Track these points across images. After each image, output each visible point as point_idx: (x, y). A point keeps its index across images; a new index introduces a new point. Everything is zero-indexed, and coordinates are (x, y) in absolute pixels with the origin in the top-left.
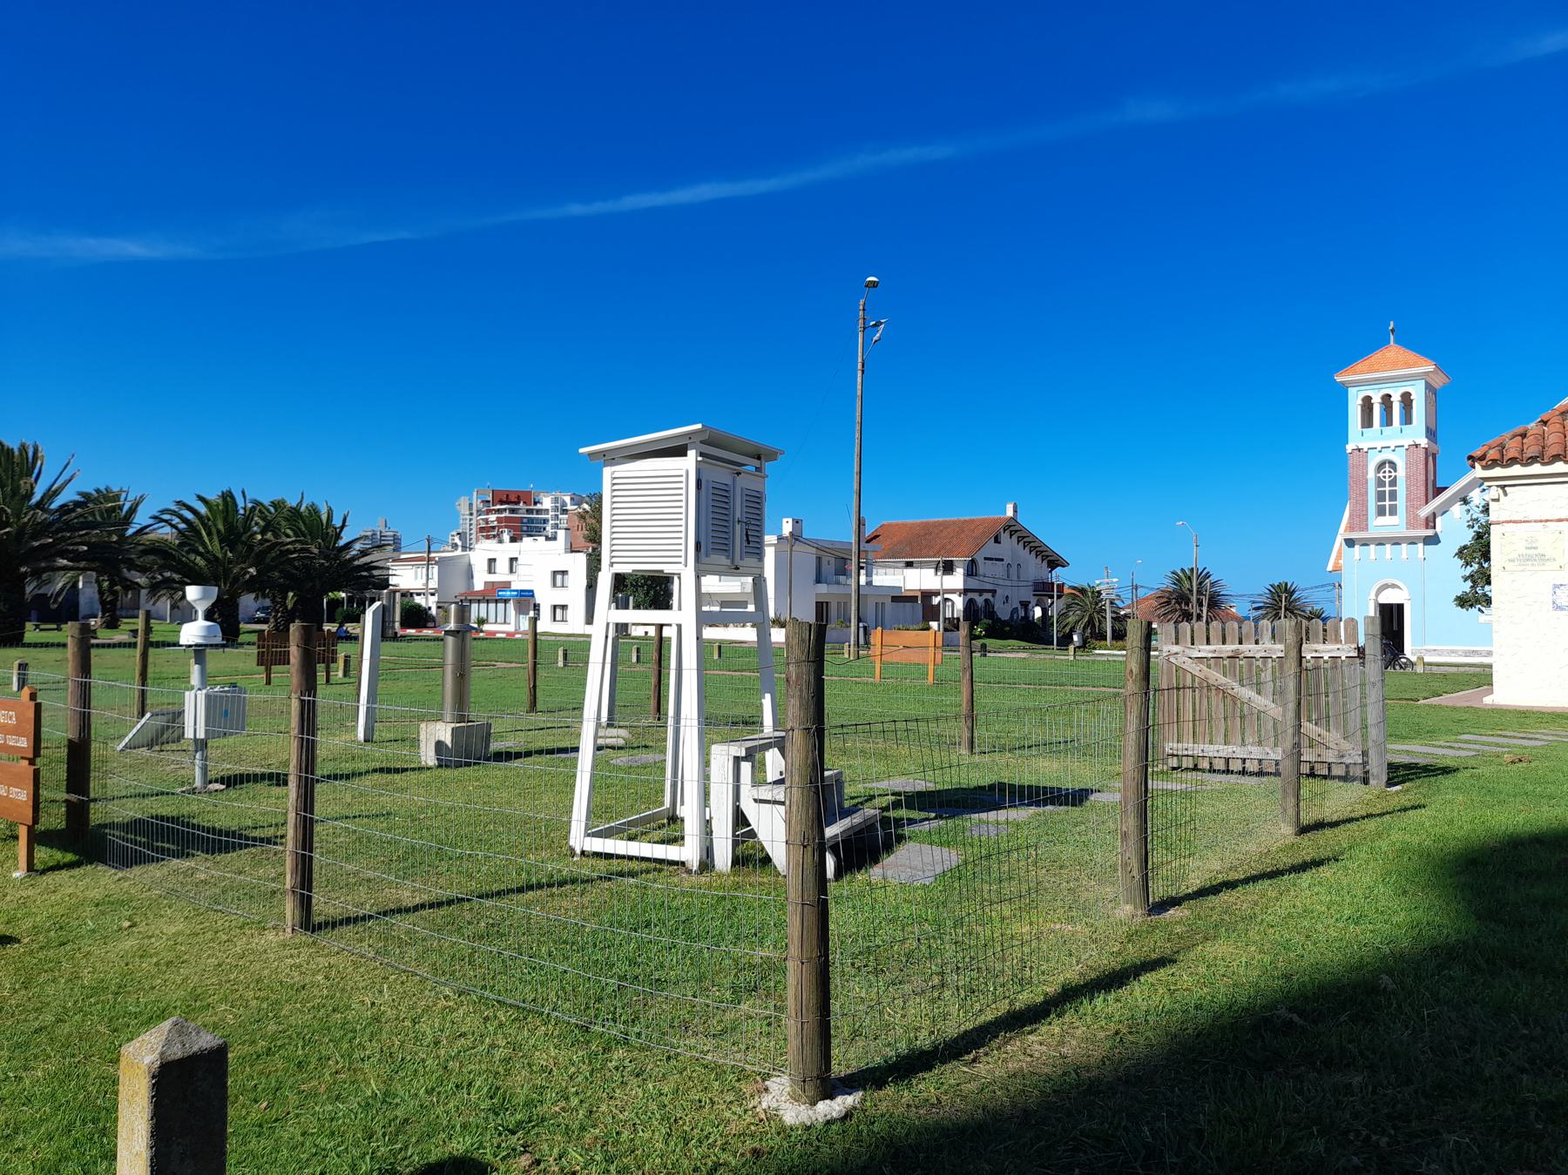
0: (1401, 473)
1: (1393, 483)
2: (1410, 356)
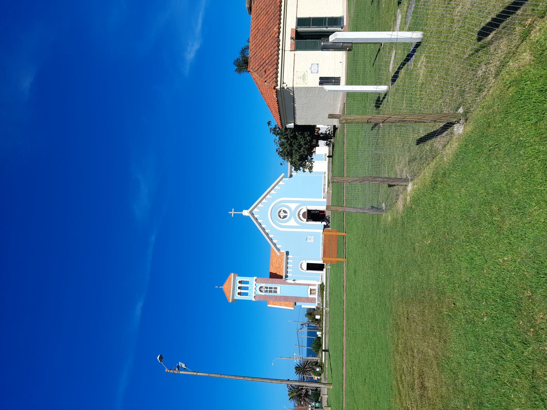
0: (264, 285)
1: (267, 288)
2: (227, 281)
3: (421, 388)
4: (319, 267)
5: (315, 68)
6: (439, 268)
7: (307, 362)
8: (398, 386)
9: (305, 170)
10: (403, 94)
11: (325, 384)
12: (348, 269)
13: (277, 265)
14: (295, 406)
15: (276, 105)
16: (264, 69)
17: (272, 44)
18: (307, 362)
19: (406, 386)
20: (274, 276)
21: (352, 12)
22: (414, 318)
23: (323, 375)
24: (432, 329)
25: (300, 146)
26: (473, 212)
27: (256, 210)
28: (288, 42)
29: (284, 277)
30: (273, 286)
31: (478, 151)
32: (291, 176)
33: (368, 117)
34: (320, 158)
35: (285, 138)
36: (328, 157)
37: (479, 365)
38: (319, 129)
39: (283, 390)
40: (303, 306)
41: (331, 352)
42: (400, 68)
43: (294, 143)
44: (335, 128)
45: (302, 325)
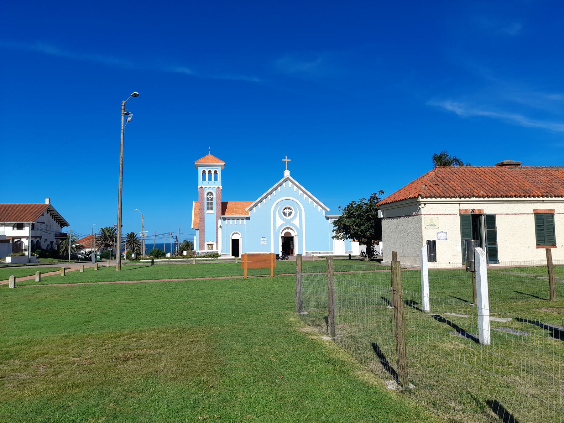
0: (214, 196)
1: (212, 199)
3: (125, 357)
4: (235, 252)
5: (442, 236)
6: (247, 370)
7: (140, 245)
8: (124, 335)
9: (335, 232)
10: (423, 328)
11: (120, 263)
12: (236, 281)
13: (235, 209)
14: (95, 235)
15: (401, 198)
16: (439, 184)
17: (466, 190)
18: (140, 245)
19: (126, 342)
20: (224, 206)
21: (505, 272)
22: (194, 348)
23: (128, 261)
24: (184, 366)
25: (359, 225)
26: (307, 402)
27: (290, 184)
28: (468, 207)
29: (224, 216)
30: (214, 206)
31: (371, 405)
32: (327, 218)
33: (399, 291)
34: (348, 247)
35: (367, 210)
36: (350, 255)
37: (154, 413)
38: (378, 244)
39: (110, 222)
40: (195, 237)
41: (152, 268)
42: (449, 323)
43: (362, 219)
44: (380, 261)
45: (176, 237)
